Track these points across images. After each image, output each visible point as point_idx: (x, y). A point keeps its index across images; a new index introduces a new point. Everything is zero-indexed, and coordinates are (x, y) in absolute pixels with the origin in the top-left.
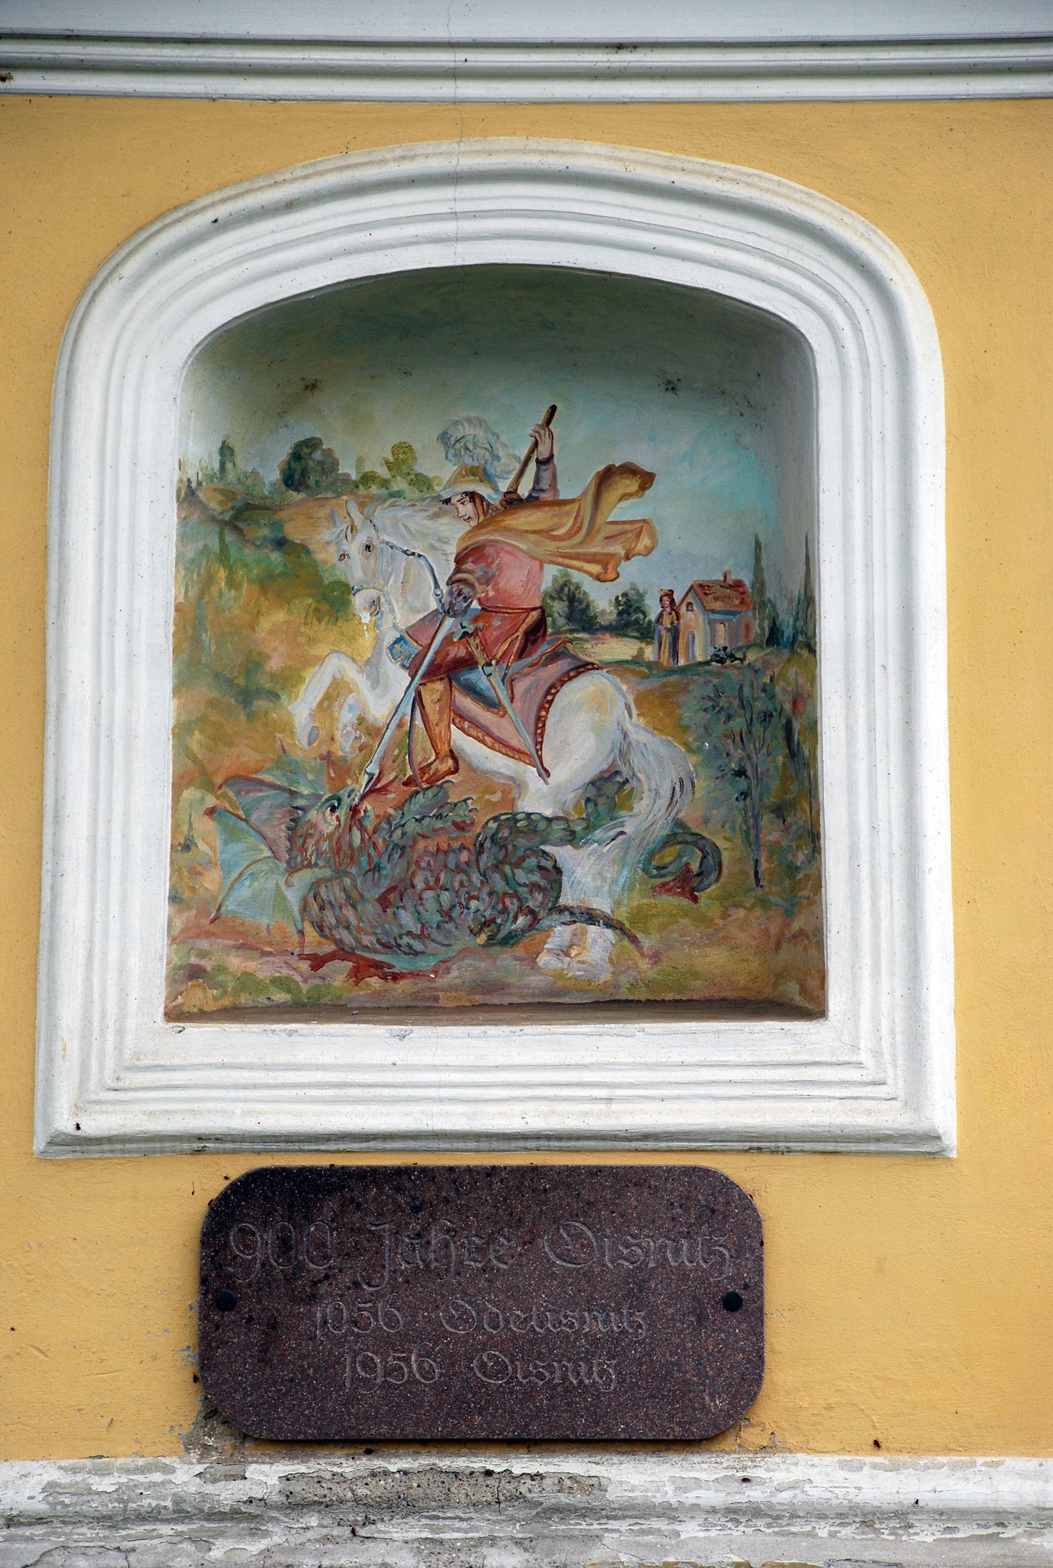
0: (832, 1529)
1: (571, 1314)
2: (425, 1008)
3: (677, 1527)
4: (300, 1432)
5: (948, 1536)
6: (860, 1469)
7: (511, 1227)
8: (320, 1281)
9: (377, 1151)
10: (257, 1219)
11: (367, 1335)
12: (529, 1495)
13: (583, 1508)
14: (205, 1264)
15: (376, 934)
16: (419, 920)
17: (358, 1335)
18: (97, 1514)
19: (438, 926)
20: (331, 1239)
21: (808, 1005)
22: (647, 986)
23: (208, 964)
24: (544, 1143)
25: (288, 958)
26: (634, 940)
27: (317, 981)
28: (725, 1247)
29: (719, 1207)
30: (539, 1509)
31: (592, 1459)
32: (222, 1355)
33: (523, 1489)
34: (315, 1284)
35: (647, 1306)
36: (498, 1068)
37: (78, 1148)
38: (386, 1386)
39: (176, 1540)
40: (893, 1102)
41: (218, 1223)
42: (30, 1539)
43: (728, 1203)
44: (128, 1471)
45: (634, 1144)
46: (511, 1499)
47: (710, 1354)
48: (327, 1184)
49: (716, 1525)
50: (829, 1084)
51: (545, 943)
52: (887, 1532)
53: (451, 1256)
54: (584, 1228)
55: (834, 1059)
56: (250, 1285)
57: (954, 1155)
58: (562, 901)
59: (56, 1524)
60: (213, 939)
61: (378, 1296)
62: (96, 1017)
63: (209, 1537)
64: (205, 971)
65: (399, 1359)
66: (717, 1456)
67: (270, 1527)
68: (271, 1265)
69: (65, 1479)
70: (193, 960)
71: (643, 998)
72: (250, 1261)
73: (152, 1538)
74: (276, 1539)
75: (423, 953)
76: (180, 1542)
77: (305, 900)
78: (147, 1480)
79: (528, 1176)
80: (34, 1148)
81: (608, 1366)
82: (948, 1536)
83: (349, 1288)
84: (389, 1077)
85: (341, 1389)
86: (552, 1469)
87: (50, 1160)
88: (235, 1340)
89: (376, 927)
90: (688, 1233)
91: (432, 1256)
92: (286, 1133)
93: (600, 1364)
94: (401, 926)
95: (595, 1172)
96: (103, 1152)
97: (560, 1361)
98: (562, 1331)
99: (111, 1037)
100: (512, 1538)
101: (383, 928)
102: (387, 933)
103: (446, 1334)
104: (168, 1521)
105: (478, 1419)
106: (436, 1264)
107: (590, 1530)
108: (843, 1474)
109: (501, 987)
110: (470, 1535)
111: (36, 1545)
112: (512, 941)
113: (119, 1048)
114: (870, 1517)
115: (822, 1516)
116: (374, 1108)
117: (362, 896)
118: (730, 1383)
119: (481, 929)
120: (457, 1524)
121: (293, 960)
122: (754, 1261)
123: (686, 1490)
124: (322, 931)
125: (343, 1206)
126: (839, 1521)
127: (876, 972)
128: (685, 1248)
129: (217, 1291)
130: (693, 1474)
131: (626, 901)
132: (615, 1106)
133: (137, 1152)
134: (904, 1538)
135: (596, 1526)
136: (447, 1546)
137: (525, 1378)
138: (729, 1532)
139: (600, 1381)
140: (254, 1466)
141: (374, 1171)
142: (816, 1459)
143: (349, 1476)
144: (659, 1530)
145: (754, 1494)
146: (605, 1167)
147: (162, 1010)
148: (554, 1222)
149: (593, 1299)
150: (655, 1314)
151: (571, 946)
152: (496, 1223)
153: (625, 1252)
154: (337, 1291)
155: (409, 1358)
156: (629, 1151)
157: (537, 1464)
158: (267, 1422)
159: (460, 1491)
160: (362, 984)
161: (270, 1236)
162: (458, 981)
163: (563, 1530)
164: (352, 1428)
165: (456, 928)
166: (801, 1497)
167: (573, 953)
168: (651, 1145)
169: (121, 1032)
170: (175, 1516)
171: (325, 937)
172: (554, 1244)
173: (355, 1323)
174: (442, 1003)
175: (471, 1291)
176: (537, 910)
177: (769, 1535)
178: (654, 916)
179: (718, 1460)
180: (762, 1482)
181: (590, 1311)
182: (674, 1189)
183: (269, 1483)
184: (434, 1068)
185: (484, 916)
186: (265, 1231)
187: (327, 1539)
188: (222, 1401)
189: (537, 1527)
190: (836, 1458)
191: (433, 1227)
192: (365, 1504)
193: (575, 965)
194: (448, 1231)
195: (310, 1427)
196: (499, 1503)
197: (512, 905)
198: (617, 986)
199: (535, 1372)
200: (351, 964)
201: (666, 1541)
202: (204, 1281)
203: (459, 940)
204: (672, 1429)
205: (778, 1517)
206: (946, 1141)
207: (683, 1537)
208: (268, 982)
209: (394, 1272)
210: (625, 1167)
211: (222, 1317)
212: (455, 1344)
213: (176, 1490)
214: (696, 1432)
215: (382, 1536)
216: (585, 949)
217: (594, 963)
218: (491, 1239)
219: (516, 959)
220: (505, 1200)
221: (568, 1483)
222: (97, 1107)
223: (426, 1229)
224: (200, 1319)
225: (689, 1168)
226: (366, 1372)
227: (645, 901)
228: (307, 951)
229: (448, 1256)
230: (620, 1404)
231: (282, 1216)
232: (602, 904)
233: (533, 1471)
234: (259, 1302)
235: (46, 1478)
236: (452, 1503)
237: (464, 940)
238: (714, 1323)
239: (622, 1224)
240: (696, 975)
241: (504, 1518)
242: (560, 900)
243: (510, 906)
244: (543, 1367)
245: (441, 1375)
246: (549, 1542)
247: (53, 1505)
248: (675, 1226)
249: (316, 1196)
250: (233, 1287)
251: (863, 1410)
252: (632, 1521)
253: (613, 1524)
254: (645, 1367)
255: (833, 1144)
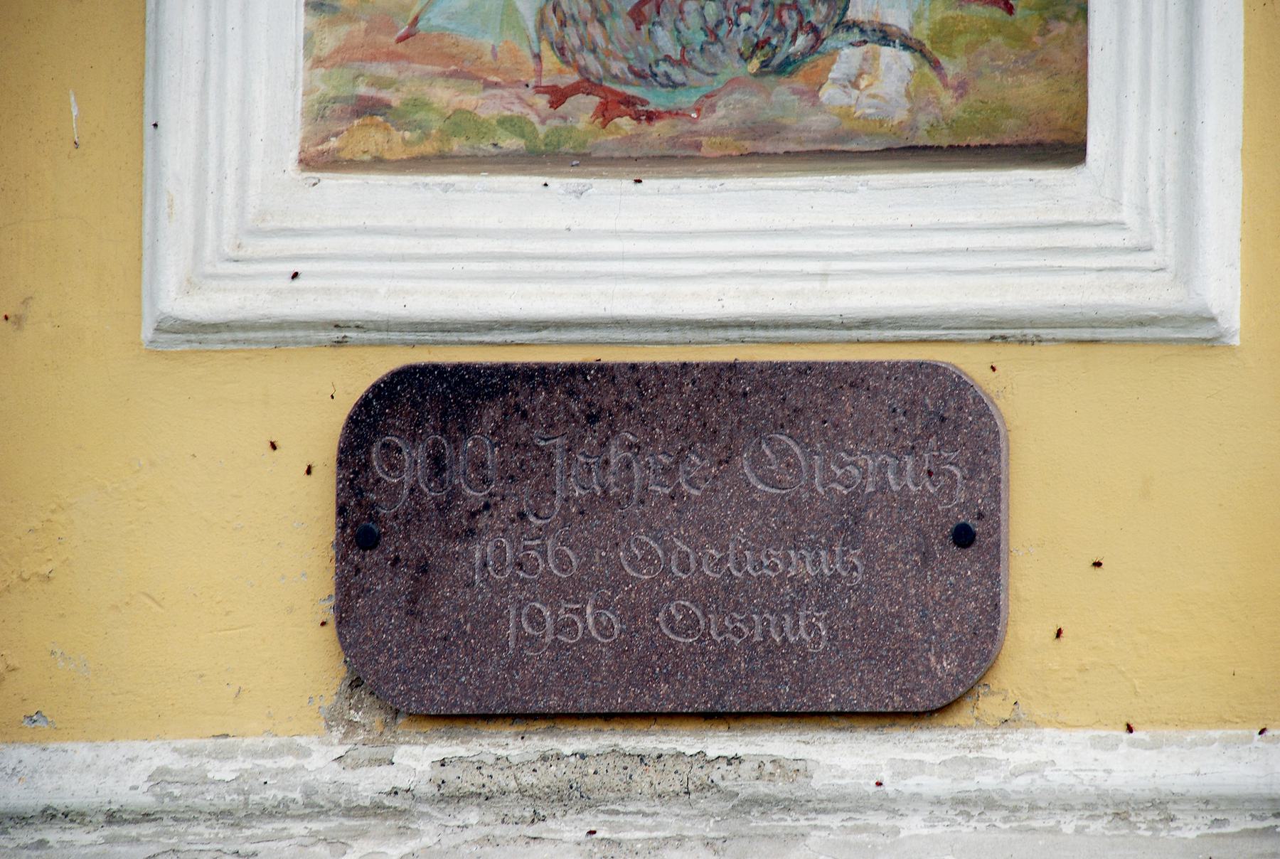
0: (1081, 823)
1: (774, 553)
2: (683, 157)
3: (899, 822)
4: (455, 705)
5: (1215, 831)
6: (1115, 747)
7: (704, 442)
8: (479, 512)
9: (551, 343)
10: (404, 431)
11: (534, 580)
12: (722, 784)
13: (785, 799)
14: (342, 490)
15: (627, 59)
16: (679, 40)
17: (523, 581)
18: (213, 809)
19: (702, 49)
20: (492, 457)
21: (1067, 149)
22: (950, 127)
23: (394, 98)
24: (747, 333)
25: (522, 91)
26: (936, 65)
27: (556, 122)
28: (956, 465)
29: (951, 414)
30: (735, 801)
31: (803, 738)
32: (363, 607)
33: (716, 776)
34: (473, 515)
35: (864, 542)
36: (693, 234)
37: (193, 337)
38: (556, 646)
39: (308, 841)
40: (1161, 274)
41: (357, 436)
42: (136, 840)
43: (961, 409)
44: (254, 754)
45: (855, 334)
46: (702, 788)
47: (936, 603)
48: (487, 387)
49: (943, 820)
50: (1084, 251)
51: (829, 70)
52: (1144, 826)
53: (633, 480)
54: (791, 443)
55: (1091, 219)
56: (396, 517)
57: (1236, 341)
58: (851, 15)
59: (167, 821)
60: (403, 64)
61: (545, 531)
62: (212, 164)
63: (348, 837)
64: (389, 106)
65: (571, 611)
66: (950, 733)
67: (421, 825)
68: (421, 491)
69: (177, 763)
70: (363, 90)
71: (945, 142)
72: (396, 486)
73: (280, 839)
74: (426, 841)
75: (683, 85)
76: (313, 844)
77: (542, 12)
78: (275, 766)
79: (726, 375)
80: (143, 336)
81: (818, 619)
82: (1215, 831)
83: (513, 521)
84: (563, 247)
85: (503, 650)
86: (753, 750)
87: (162, 352)
88: (379, 588)
89: (627, 50)
90: (913, 448)
91: (612, 479)
92: (438, 320)
93: (807, 616)
94: (657, 49)
95: (804, 369)
96: (224, 342)
97: (761, 613)
98: (763, 575)
99: (230, 190)
100: (704, 838)
101: (637, 52)
102: (640, 58)
103: (627, 579)
104: (302, 817)
105: (664, 687)
106: (616, 489)
107: (796, 828)
108: (1093, 753)
109: (773, 130)
110: (654, 834)
111: (141, 848)
112: (790, 69)
113: (241, 205)
114: (1124, 808)
115: (1067, 808)
116: (546, 287)
117: (610, 7)
118: (960, 640)
119: (753, 52)
120: (641, 820)
121: (528, 94)
122: (990, 483)
123: (905, 776)
124: (563, 54)
125: (505, 414)
126: (1088, 813)
127: (1144, 104)
128: (908, 467)
129: (356, 524)
130: (917, 756)
131: (927, 14)
132: (832, 284)
133: (266, 342)
134: (1163, 834)
135: (803, 822)
136: (624, 848)
137: (720, 634)
138: (958, 828)
139: (808, 639)
140: (404, 748)
141: (543, 369)
142: (1064, 735)
143: (515, 760)
144: (877, 826)
145: (987, 781)
146: (815, 363)
147: (294, 155)
148: (756, 435)
149: (800, 533)
150: (873, 552)
151: (860, 75)
152: (687, 437)
153: (839, 472)
154: (498, 525)
155: (584, 610)
156: (849, 342)
157: (735, 744)
158: (418, 692)
159: (643, 779)
160: (611, 126)
161: (420, 453)
162: (725, 122)
163: (765, 828)
164: (516, 700)
165: (724, 51)
166: (1040, 782)
167: (863, 84)
168: (874, 334)
169: (242, 183)
170: (308, 810)
171: (567, 63)
172: (755, 463)
173: (520, 565)
174: (705, 151)
175: (657, 524)
176: (820, 26)
177: (1005, 831)
178: (960, 32)
179: (950, 737)
180: (996, 764)
181: (797, 548)
182: (897, 392)
183: (419, 768)
184: (616, 234)
185: (756, 35)
186: (413, 447)
187: (488, 839)
188: (363, 665)
189: (734, 824)
190: (1090, 733)
191: (613, 442)
192: (531, 796)
193: (865, 101)
194: (630, 447)
195: (466, 697)
196: (688, 793)
197: (790, 19)
198: (914, 128)
199: (731, 627)
200: (597, 99)
201: (881, 840)
202: (341, 510)
203: (726, 67)
204: (892, 698)
205: (1016, 809)
206: (1223, 324)
207: (901, 836)
208: (494, 122)
209: (567, 500)
210: (839, 363)
211: (363, 557)
212: (638, 592)
213: (307, 778)
214: (920, 703)
215: (552, 836)
216: (877, 78)
217: (888, 98)
218: (681, 457)
219: (795, 92)
220: (698, 407)
221: (769, 767)
222: (215, 283)
223: (603, 445)
224: (337, 561)
225: (915, 364)
226: (533, 628)
227: (950, 13)
228: (545, 82)
229: (630, 480)
230: (831, 668)
231: (434, 428)
232: (899, 19)
233: (730, 754)
234: (407, 538)
235: (157, 763)
236: (633, 794)
237: (732, 67)
238: (941, 563)
239: (835, 436)
240: (1007, 111)
241: (695, 812)
242: (849, 13)
243: (788, 22)
244: (741, 621)
245: (621, 631)
246: (744, 842)
247: (160, 798)
248: (897, 439)
249: (474, 401)
250: (375, 518)
251: (1121, 672)
252: (845, 815)
253: (823, 820)
254: (860, 620)
255: (1090, 330)
